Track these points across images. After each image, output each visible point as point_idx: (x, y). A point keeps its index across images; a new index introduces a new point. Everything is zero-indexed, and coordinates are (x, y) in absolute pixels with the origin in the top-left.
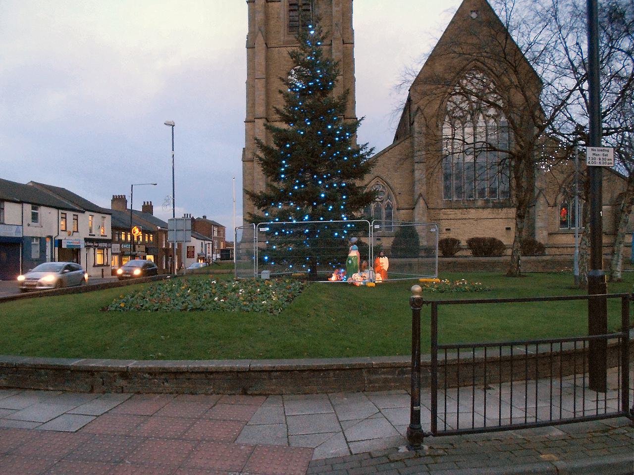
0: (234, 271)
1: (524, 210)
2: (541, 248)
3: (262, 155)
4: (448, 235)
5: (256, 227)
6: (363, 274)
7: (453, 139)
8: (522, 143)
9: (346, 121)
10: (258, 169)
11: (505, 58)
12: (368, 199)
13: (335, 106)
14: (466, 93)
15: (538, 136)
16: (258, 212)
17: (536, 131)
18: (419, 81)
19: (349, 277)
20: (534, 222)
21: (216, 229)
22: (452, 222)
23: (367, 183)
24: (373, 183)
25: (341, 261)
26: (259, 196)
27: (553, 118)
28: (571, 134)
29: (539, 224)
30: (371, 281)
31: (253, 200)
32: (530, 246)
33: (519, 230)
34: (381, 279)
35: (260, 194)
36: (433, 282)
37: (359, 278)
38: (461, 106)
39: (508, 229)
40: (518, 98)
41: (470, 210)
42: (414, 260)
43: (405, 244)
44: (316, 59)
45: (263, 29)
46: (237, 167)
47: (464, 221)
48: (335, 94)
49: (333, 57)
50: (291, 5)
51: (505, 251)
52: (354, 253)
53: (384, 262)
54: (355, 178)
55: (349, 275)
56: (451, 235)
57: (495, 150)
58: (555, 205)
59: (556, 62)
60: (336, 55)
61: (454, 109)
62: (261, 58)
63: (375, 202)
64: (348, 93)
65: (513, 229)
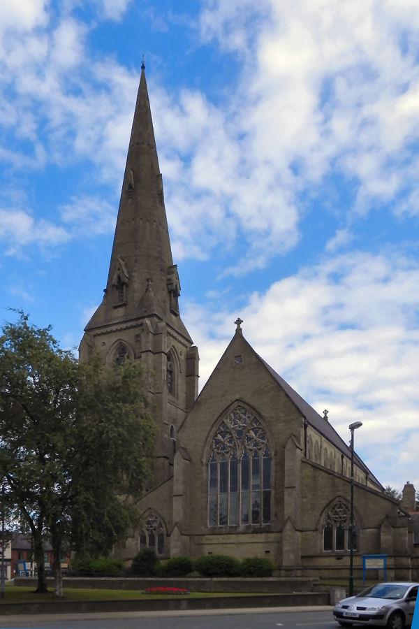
47: (225, 546)
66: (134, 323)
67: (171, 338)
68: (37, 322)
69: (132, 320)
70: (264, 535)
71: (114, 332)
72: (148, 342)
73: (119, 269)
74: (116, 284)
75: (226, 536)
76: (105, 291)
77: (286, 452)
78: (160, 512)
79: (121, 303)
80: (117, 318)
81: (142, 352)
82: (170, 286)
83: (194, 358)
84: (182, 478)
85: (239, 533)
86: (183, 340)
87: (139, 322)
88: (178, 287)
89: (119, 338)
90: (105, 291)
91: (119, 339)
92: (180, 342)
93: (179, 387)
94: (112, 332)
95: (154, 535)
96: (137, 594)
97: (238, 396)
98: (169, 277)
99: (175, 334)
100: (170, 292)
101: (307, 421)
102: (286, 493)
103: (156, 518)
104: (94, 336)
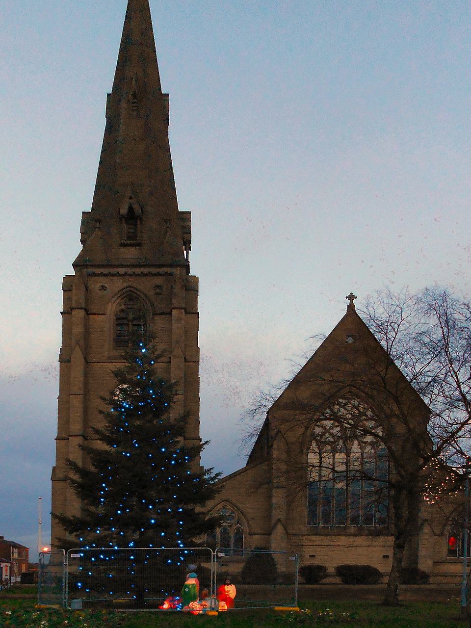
0: (38, 596)
1: (404, 535)
2: (424, 577)
3: (76, 477)
4: (312, 561)
5: (66, 553)
6: (203, 603)
7: (320, 466)
8: (403, 473)
9: (187, 442)
10: (71, 493)
11: (385, 387)
12: (210, 526)
13: (172, 427)
14: (336, 418)
15: (421, 467)
16: (71, 538)
17: (421, 461)
18: (279, 405)
19: (185, 606)
20: (417, 549)
21: (16, 550)
23: (212, 508)
24: (219, 507)
25: (177, 588)
26: (71, 520)
27: (440, 449)
28: (460, 468)
29: (422, 552)
30: (213, 609)
31: (64, 525)
32: (410, 574)
33: (398, 561)
34: (226, 608)
35: (72, 518)
36: (290, 612)
37: (197, 606)
38: (331, 431)
39: (386, 557)
40: (400, 429)
41: (340, 537)
42: (270, 587)
43: (259, 570)
44: (148, 378)
45: (82, 342)
46: (47, 486)
48: (174, 414)
49: (172, 375)
50: (118, 319)
51: (382, 579)
52: (192, 581)
53: (231, 590)
54: (195, 503)
55: (185, 602)
56: (316, 562)
57: (370, 479)
58: (442, 534)
59: (447, 394)
60: (176, 374)
61: (324, 434)
62: (78, 373)
63: (221, 526)
64: (191, 415)
65: (391, 559)
66: (154, 270)
81: (174, 309)
85: (351, 535)
89: (130, 284)
91: (130, 286)
94: (118, 274)
104: (89, 275)
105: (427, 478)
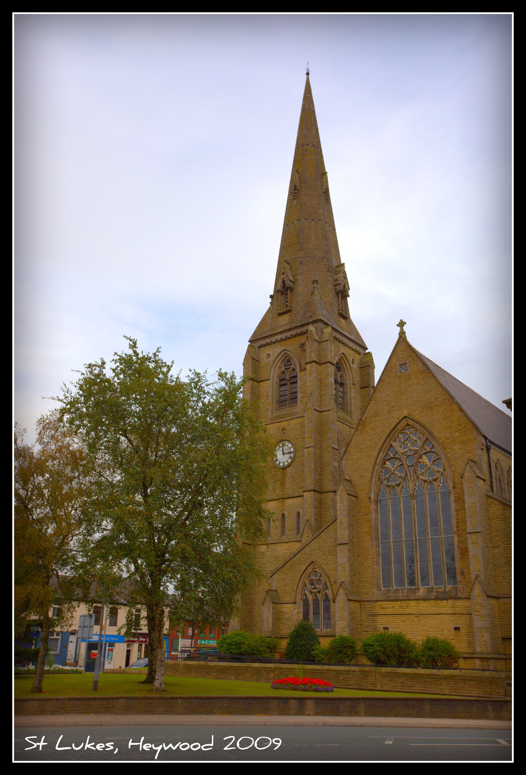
5: (254, 744)
22: (390, 618)
39: (457, 629)
41: (409, 602)
47: (403, 618)
50: (281, 380)
66: (298, 331)
67: (341, 345)
68: (145, 349)
69: (296, 328)
70: (450, 602)
71: (280, 341)
72: (311, 354)
73: (283, 274)
74: (281, 289)
75: (403, 603)
76: (271, 297)
77: (465, 484)
78: (325, 567)
79: (285, 310)
80: (280, 326)
81: (307, 363)
82: (337, 287)
83: (371, 365)
84: (347, 519)
86: (354, 346)
87: (304, 329)
88: (347, 287)
90: (271, 297)
91: (284, 350)
92: (350, 348)
93: (353, 401)
95: (318, 601)
96: (263, 689)
97: (405, 412)
98: (336, 276)
99: (345, 340)
100: (337, 294)
101: (490, 442)
102: (469, 541)
103: (321, 576)
105: (26, 507)
